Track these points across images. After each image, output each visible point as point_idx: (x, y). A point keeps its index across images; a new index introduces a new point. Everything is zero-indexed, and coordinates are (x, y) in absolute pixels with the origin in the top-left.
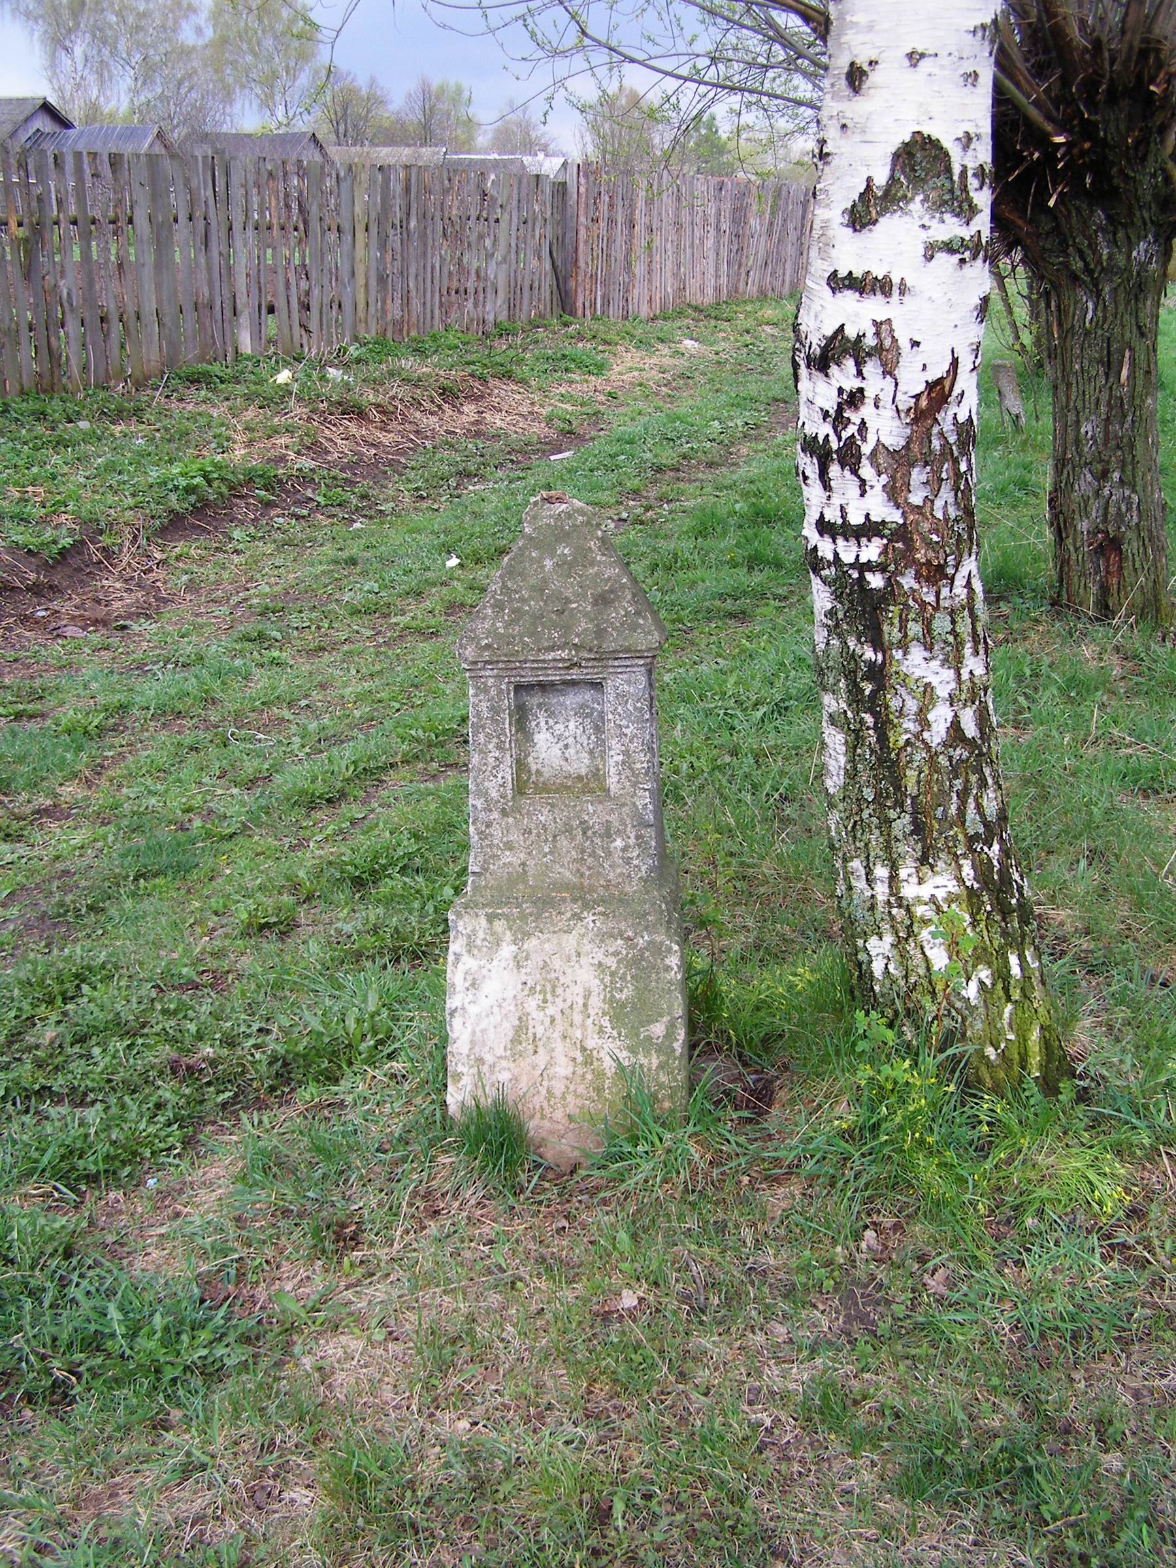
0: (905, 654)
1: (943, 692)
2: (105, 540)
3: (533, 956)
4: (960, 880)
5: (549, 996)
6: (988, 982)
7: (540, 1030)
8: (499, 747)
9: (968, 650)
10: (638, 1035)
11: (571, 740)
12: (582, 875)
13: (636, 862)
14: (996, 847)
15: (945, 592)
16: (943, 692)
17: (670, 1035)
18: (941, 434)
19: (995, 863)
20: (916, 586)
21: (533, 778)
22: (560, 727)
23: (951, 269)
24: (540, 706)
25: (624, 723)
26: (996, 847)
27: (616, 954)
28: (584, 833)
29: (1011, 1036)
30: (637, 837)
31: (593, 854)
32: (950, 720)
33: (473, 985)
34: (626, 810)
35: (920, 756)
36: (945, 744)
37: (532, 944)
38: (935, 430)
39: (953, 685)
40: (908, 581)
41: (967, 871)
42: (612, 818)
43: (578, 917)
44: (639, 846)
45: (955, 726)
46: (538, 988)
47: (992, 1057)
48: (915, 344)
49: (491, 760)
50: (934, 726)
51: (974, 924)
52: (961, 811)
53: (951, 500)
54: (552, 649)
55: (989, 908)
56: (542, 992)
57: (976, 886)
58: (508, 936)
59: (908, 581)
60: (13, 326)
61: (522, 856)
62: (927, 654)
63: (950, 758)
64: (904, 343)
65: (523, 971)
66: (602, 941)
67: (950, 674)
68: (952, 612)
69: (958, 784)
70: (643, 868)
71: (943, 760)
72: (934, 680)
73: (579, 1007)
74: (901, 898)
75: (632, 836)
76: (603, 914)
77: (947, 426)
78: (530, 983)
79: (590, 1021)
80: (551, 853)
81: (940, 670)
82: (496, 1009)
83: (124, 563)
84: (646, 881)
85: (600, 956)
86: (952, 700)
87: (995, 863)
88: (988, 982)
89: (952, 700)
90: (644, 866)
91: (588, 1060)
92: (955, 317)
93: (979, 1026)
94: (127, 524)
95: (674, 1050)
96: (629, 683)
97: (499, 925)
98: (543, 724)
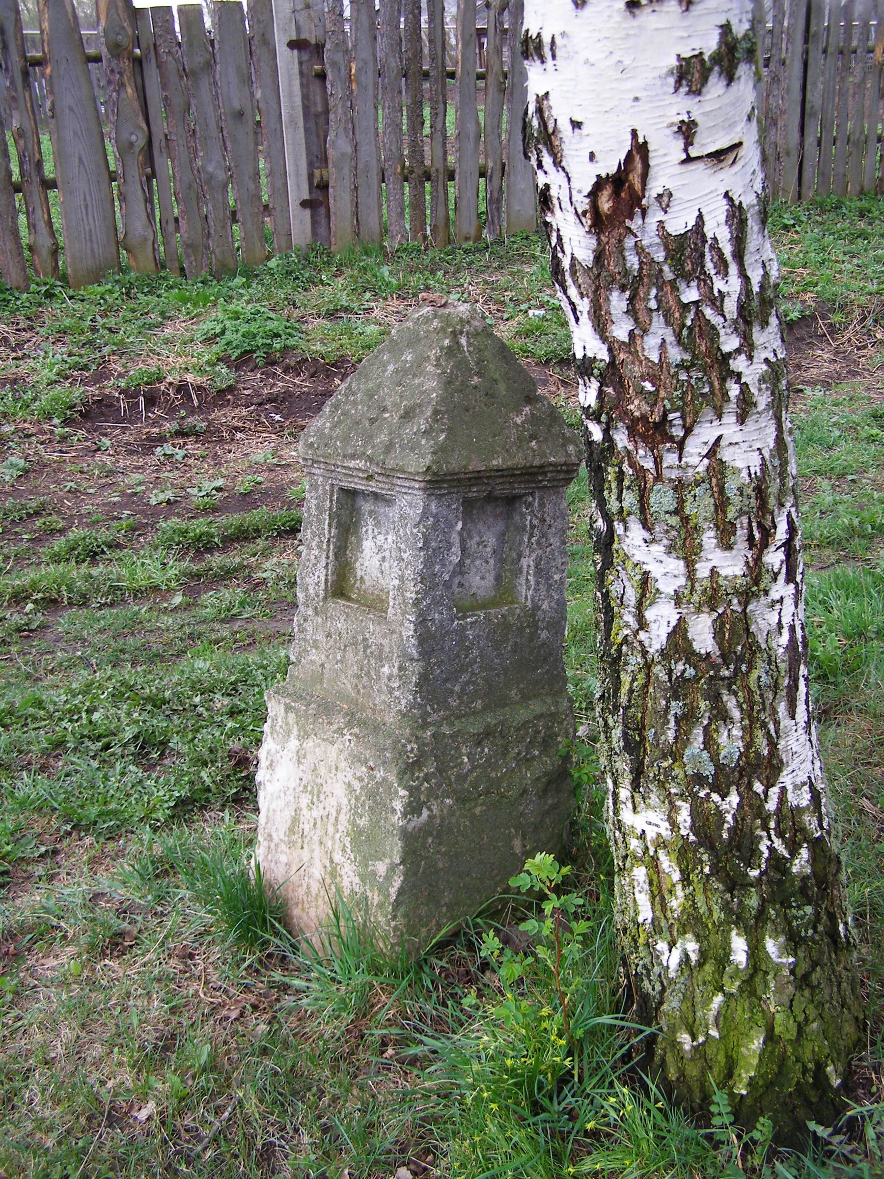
0: (626, 529)
1: (667, 586)
2: (836, 318)
3: (308, 756)
4: (674, 825)
5: (315, 800)
6: (694, 957)
7: (307, 827)
8: (319, 547)
9: (709, 539)
10: (366, 865)
11: (387, 554)
12: (359, 691)
13: (397, 693)
14: (734, 799)
15: (670, 459)
16: (667, 586)
17: (388, 878)
18: (639, 249)
19: (729, 818)
20: (631, 447)
21: (358, 584)
22: (381, 538)
23: (617, 18)
24: (371, 513)
25: (403, 546)
26: (734, 799)
27: (361, 779)
28: (365, 651)
29: (714, 1032)
30: (401, 668)
31: (368, 674)
32: (673, 623)
33: (271, 765)
34: (395, 636)
35: (635, 660)
36: (662, 652)
37: (309, 744)
38: (629, 242)
39: (682, 581)
40: (621, 439)
41: (684, 816)
42: (385, 642)
43: (340, 731)
44: (401, 678)
45: (679, 632)
46: (309, 788)
47: (687, 1047)
48: (576, 125)
49: (313, 557)
50: (653, 627)
51: (686, 880)
52: (683, 739)
53: (670, 339)
54: (353, 457)
55: (707, 870)
56: (311, 793)
57: (692, 838)
58: (295, 731)
59: (621, 439)
60: (863, 138)
61: (323, 657)
62: (647, 535)
63: (670, 672)
64: (564, 126)
65: (301, 767)
66: (353, 763)
67: (677, 566)
68: (679, 486)
69: (676, 707)
70: (403, 702)
71: (659, 671)
72: (655, 570)
73: (332, 819)
74: (619, 821)
75: (396, 665)
76: (356, 736)
77: (650, 237)
78: (305, 782)
79: (338, 836)
80: (341, 661)
81: (664, 558)
82: (282, 795)
83: (846, 338)
84: (404, 716)
85: (350, 777)
86: (678, 599)
87: (729, 818)
88: (694, 957)
89: (678, 599)
90: (405, 699)
91: (334, 874)
92: (634, 86)
93: (675, 1004)
94: (859, 306)
95: (389, 895)
96: (410, 506)
97: (292, 716)
98: (370, 531)
